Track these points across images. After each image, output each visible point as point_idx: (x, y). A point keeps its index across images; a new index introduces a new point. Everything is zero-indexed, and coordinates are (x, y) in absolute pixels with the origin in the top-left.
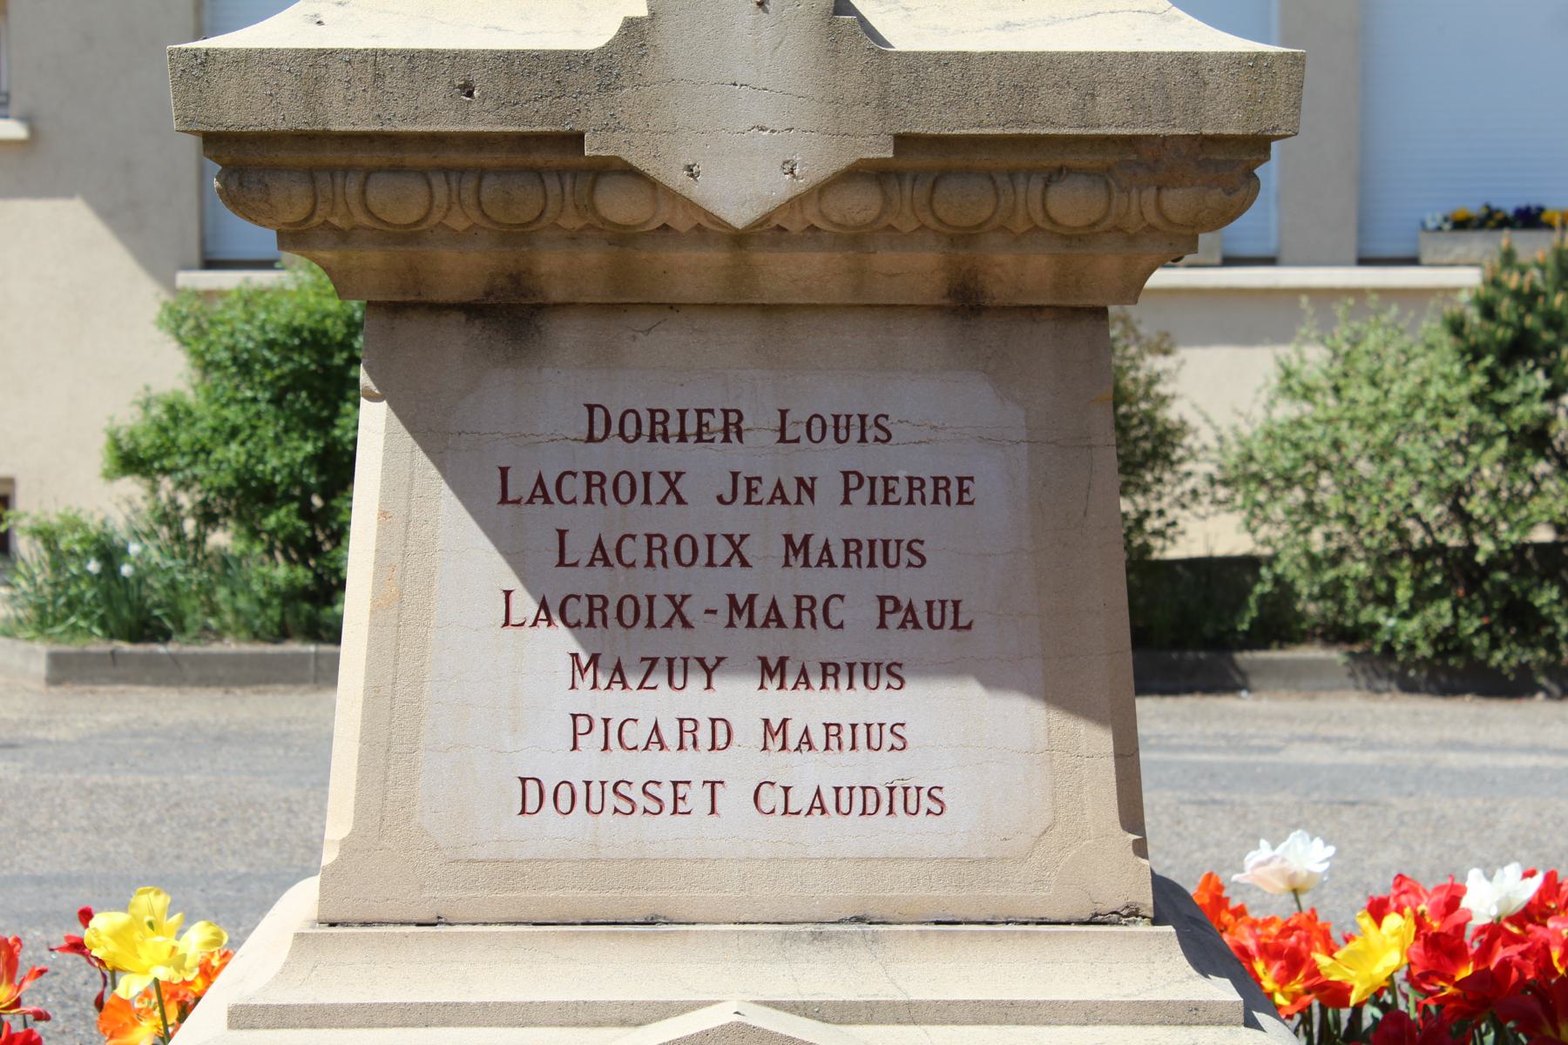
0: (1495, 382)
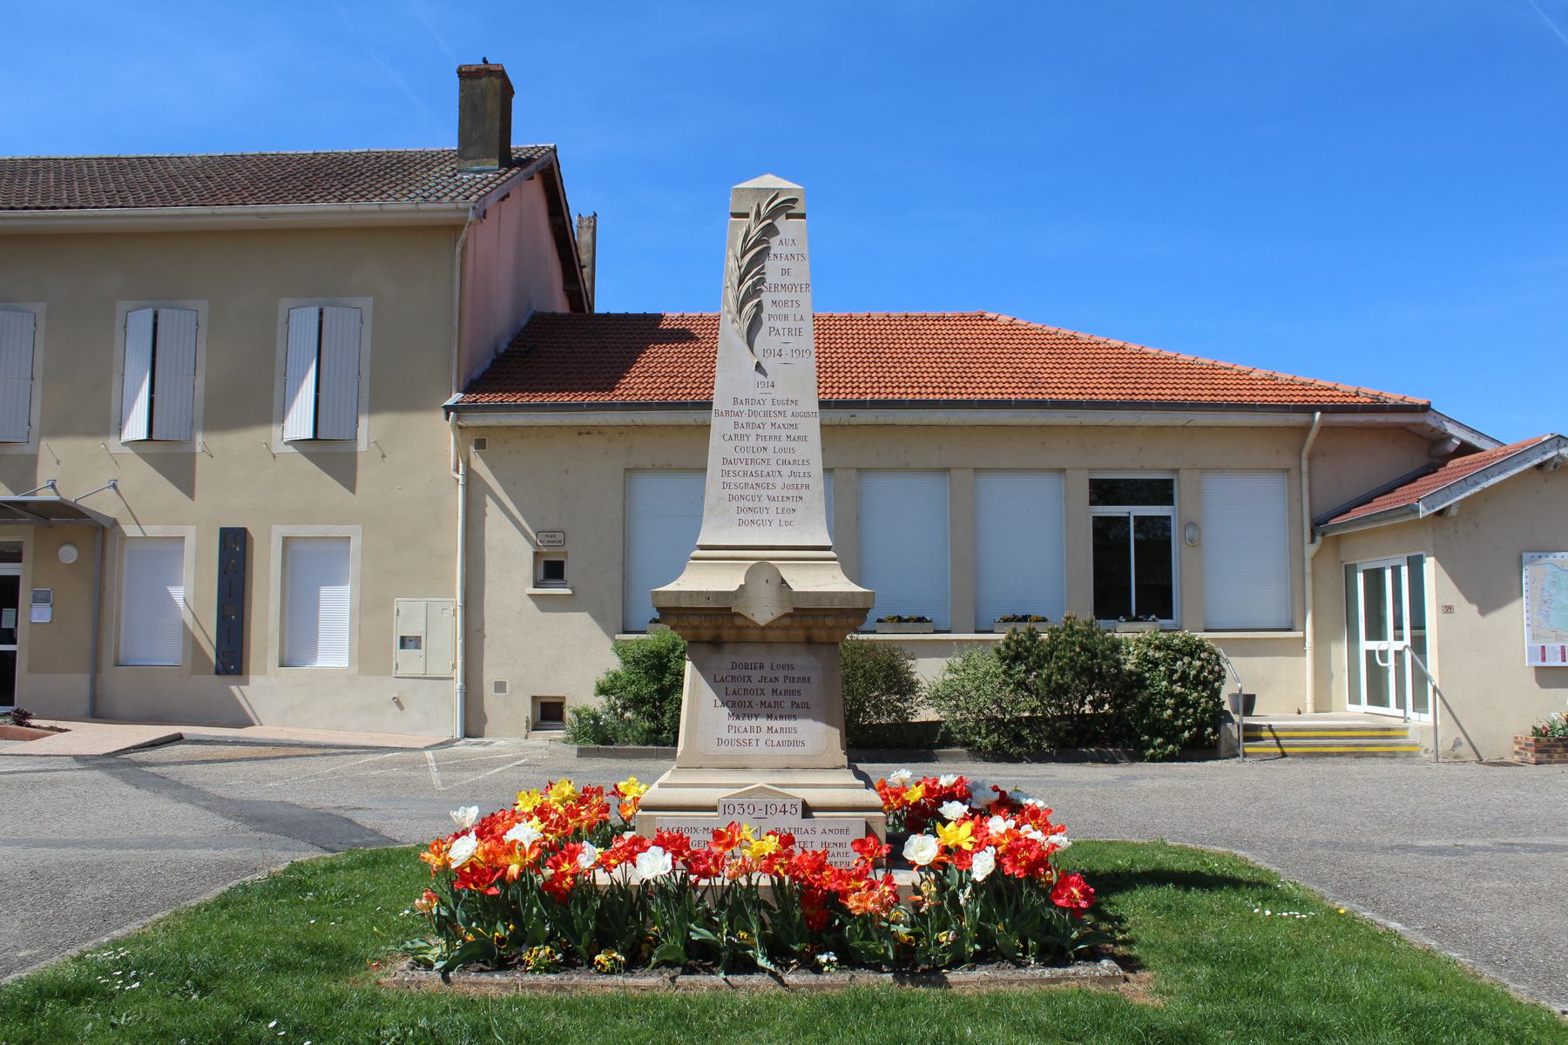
0: (1010, 667)
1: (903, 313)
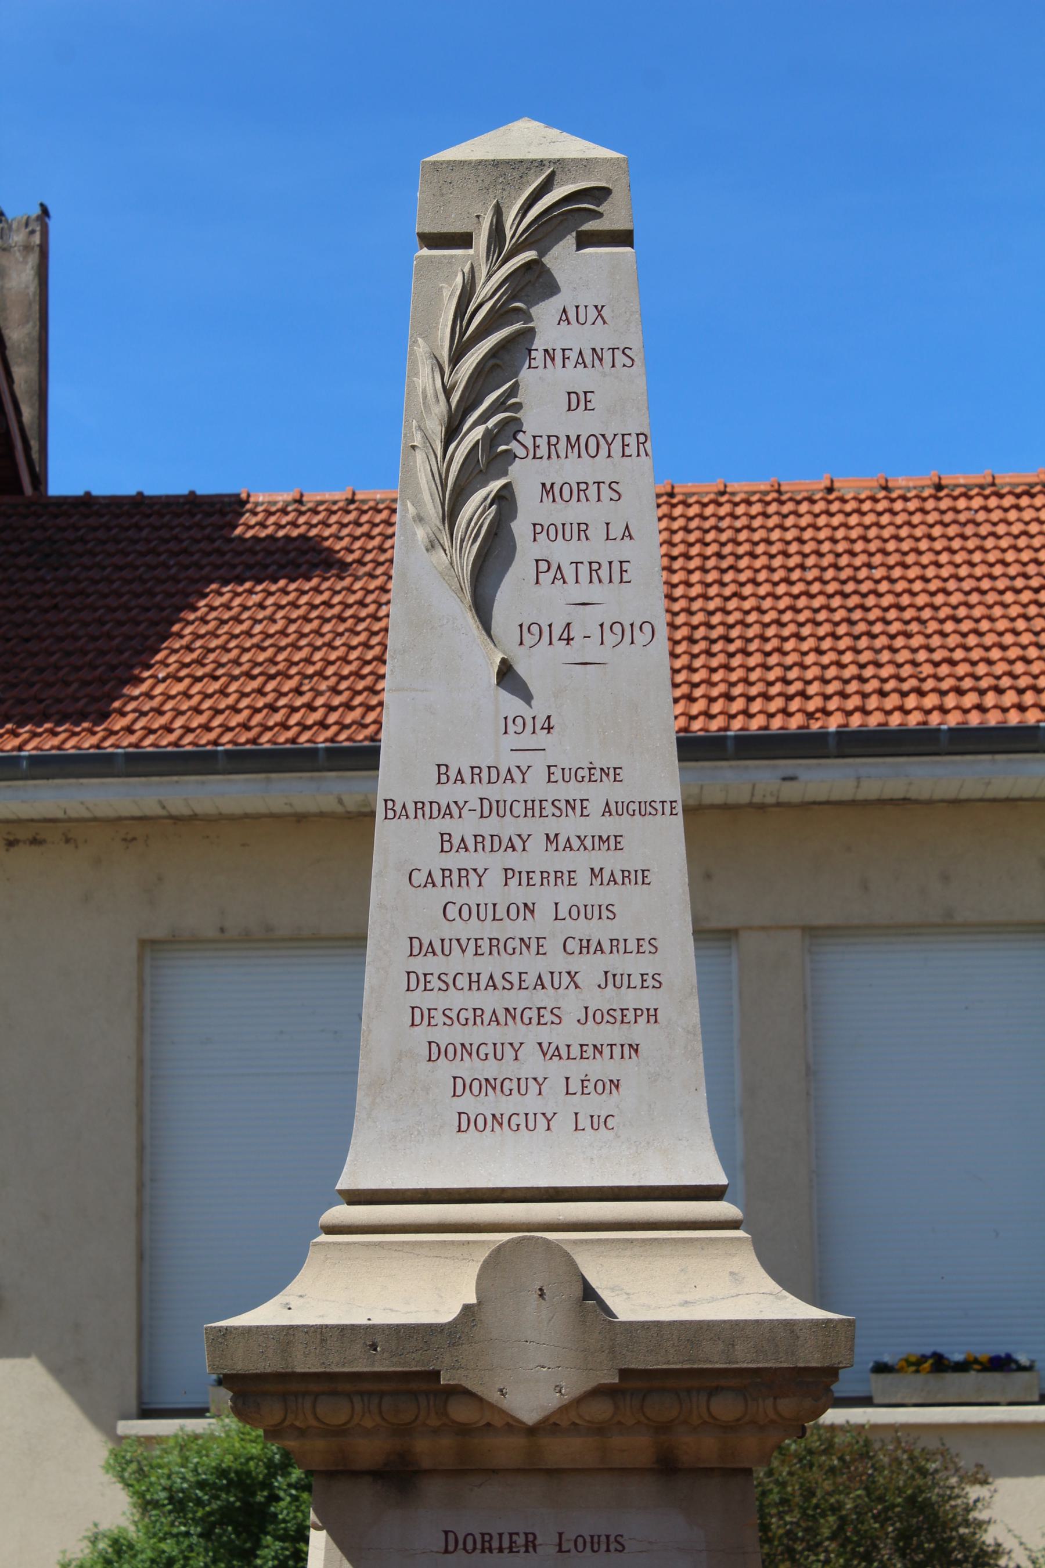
1: (929, 478)
